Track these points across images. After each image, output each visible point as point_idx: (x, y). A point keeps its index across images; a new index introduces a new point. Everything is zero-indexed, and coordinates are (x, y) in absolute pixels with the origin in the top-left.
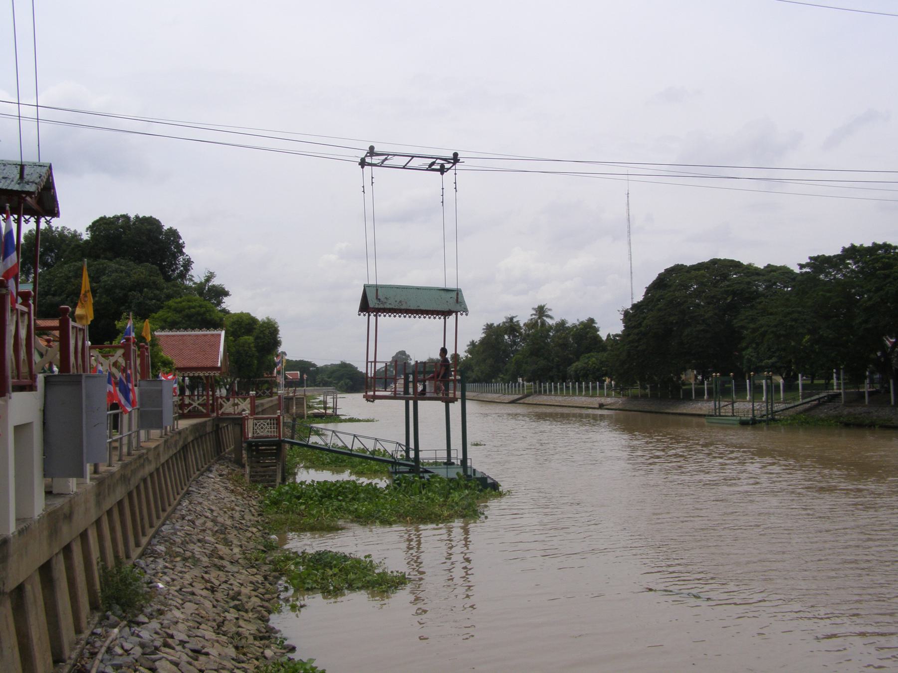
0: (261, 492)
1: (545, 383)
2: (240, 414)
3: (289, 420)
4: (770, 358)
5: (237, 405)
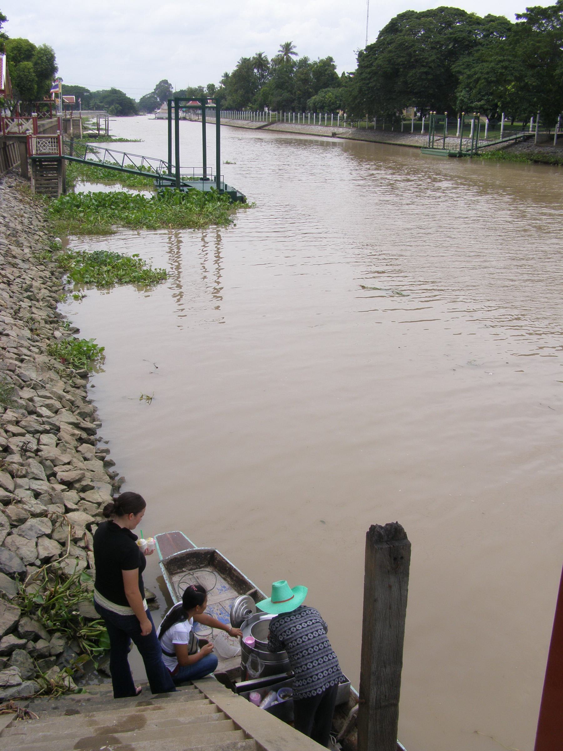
0: (46, 202)
1: (287, 113)
2: (24, 133)
3: (67, 140)
4: (479, 100)
5: (21, 125)
